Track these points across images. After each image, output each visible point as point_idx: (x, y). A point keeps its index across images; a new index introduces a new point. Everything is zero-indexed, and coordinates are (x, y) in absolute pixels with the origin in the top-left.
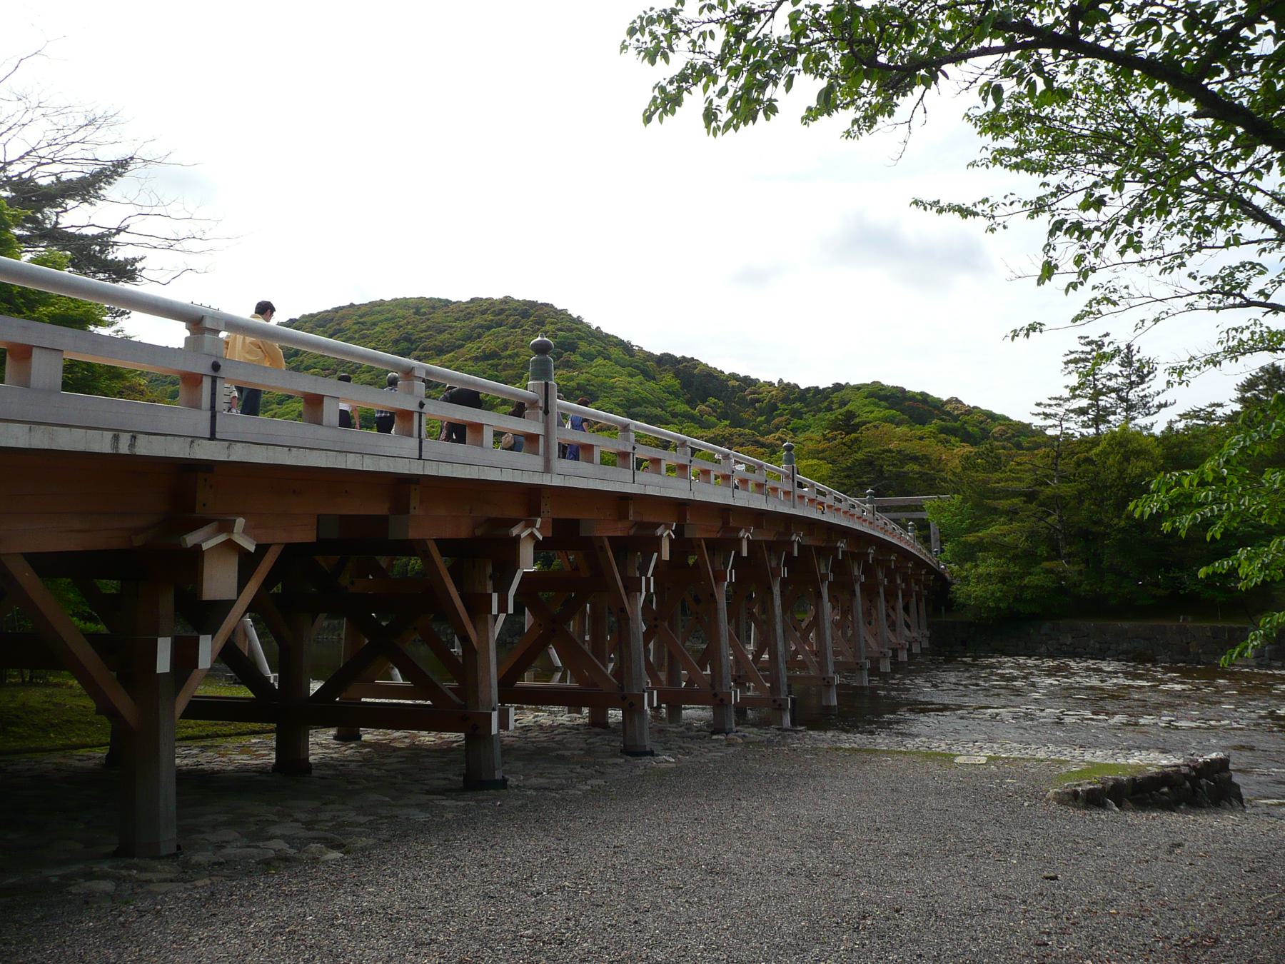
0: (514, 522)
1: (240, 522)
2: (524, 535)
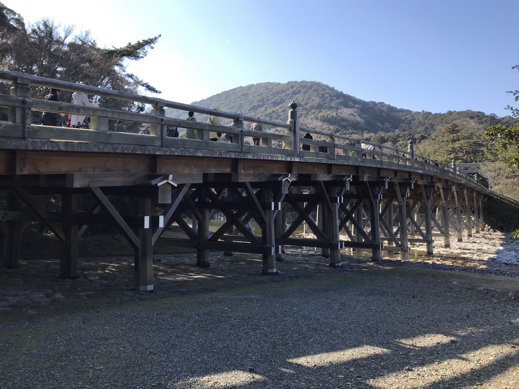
0: (279, 175)
1: (171, 177)
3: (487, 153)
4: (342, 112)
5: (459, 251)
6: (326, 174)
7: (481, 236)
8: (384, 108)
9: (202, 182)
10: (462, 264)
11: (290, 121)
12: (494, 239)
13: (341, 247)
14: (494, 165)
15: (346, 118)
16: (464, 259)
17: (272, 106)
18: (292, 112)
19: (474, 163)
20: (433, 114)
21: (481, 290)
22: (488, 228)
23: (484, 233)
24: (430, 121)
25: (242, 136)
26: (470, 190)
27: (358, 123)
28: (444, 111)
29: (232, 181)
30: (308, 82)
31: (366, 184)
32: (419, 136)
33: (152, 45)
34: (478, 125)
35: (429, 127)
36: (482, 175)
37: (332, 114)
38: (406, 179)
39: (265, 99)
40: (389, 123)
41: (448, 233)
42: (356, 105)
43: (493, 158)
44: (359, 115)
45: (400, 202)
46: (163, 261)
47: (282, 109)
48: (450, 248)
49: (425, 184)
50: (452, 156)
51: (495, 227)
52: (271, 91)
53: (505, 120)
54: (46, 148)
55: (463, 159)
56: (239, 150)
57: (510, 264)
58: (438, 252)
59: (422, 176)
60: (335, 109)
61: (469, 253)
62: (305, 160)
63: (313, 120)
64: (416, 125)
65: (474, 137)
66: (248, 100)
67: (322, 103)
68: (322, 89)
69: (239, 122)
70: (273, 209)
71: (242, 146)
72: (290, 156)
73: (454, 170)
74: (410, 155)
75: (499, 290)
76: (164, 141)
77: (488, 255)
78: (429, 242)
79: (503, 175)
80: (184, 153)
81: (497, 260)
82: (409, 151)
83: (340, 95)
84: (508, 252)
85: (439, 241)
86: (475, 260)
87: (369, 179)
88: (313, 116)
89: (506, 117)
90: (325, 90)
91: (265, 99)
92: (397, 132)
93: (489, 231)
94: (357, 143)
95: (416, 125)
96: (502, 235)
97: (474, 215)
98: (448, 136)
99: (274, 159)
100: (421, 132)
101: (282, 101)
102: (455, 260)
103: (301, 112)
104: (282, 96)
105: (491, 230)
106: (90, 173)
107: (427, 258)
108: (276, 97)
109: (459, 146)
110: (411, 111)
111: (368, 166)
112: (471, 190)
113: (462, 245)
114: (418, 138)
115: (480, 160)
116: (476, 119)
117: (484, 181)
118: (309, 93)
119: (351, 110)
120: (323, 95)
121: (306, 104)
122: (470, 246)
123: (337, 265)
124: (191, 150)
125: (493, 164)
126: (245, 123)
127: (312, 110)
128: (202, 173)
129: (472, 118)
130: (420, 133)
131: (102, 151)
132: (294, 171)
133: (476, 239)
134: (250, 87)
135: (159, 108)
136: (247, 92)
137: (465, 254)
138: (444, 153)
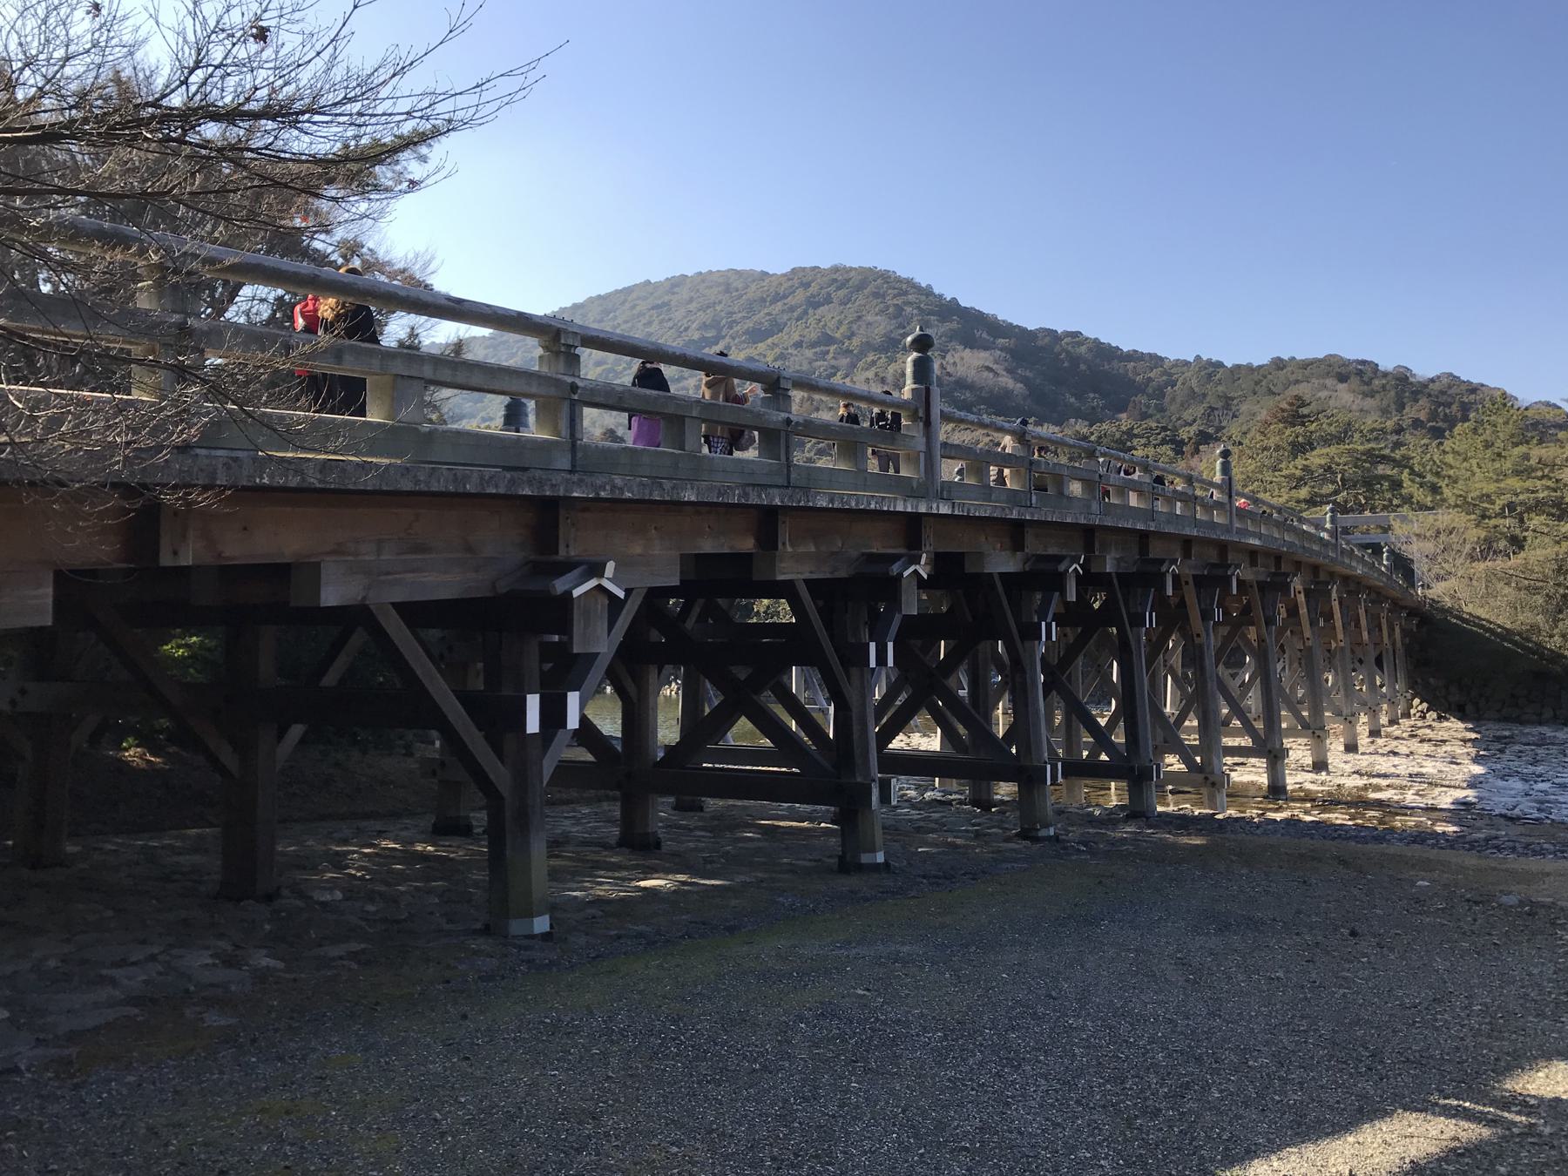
0: (894, 558)
1: (610, 568)
2: (1070, 570)
3: (1409, 483)
4: (957, 361)
6: (1008, 552)
8: (1083, 349)
9: (678, 584)
10: (1381, 822)
12: (1446, 741)
14: (1431, 519)
15: (969, 380)
16: (1379, 804)
17: (744, 342)
18: (916, 363)
19: (1367, 513)
20: (1229, 365)
21: (1511, 903)
22: (1420, 708)
23: (1412, 723)
24: (1220, 388)
25: (787, 436)
26: (1373, 596)
27: (1007, 393)
28: (1260, 358)
29: (754, 579)
30: (851, 269)
33: (423, 150)
35: (1220, 405)
36: (1400, 549)
38: (1214, 566)
40: (1097, 395)
42: (1001, 341)
43: (1429, 499)
44: (1008, 371)
47: (777, 351)
48: (1328, 773)
49: (1262, 578)
50: (1304, 493)
51: (1446, 706)
52: (740, 296)
53: (1435, 387)
54: (266, 481)
55: (1334, 502)
56: (781, 481)
57: (1519, 818)
58: (1298, 786)
59: (1253, 555)
61: (1388, 786)
62: (966, 510)
63: (871, 381)
64: (1179, 400)
65: (1357, 436)
66: (670, 324)
67: (895, 335)
68: (896, 291)
69: (780, 391)
71: (789, 467)
72: (915, 497)
74: (1222, 492)
76: (579, 455)
77: (1446, 792)
80: (647, 491)
81: (1478, 807)
82: (1218, 478)
83: (950, 310)
84: (1501, 783)
85: (1299, 752)
86: (1413, 808)
88: (870, 374)
89: (1439, 377)
90: (906, 293)
92: (1125, 421)
93: (1424, 718)
94: (1087, 458)
95: (1179, 400)
97: (1383, 672)
98: (1281, 432)
99: (885, 509)
101: (776, 327)
102: (1355, 808)
103: (833, 362)
104: (774, 312)
106: (367, 558)
107: (1271, 806)
109: (1323, 462)
110: (1161, 359)
111: (1125, 526)
112: (1377, 595)
113: (1363, 762)
114: (1190, 439)
116: (1355, 381)
117: (1403, 565)
118: (857, 304)
119: (984, 354)
120: (899, 309)
122: (1384, 765)
123: (1043, 833)
124: (667, 484)
125: (1428, 518)
126: (797, 395)
127: (866, 356)
128: (678, 553)
129: (1343, 378)
130: (1191, 425)
131: (426, 489)
132: (928, 546)
133: (1395, 743)
134: (676, 283)
135: (563, 349)
136: (666, 298)
137: (1378, 789)
138: (1279, 484)
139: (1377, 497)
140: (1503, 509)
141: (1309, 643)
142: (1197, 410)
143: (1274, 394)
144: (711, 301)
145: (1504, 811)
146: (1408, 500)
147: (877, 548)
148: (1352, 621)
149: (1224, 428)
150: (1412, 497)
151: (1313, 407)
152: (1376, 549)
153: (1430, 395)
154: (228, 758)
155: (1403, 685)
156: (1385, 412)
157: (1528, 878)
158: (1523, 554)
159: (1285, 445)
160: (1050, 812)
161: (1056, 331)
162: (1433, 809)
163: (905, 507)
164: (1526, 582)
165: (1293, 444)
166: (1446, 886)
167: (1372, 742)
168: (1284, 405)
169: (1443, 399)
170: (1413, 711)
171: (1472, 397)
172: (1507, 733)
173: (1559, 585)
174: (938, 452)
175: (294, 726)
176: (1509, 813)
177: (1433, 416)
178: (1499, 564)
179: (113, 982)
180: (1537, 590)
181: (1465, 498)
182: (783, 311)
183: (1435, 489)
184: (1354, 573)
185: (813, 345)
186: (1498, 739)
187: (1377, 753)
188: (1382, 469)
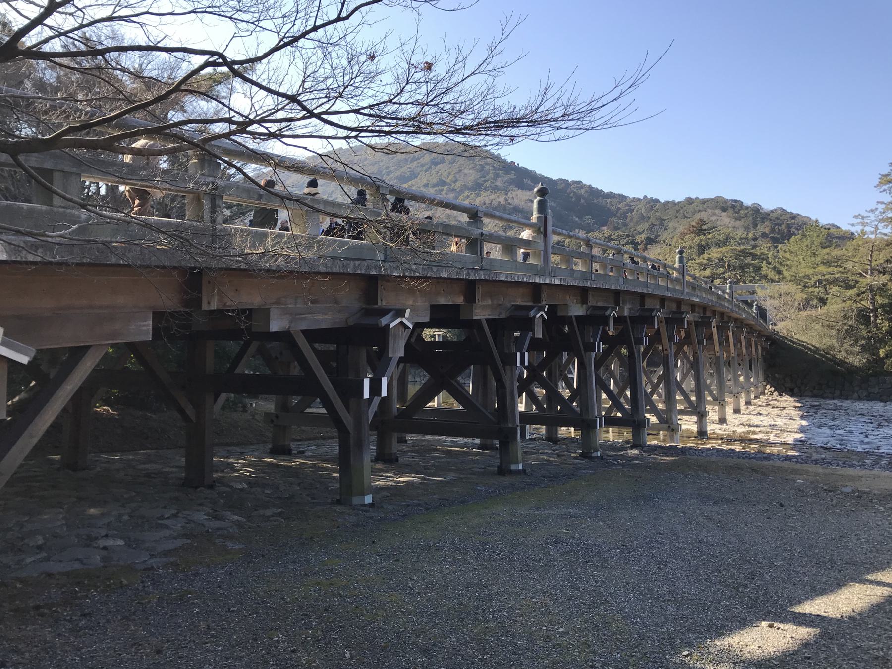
0: (530, 308)
2: (537, 316)
5: (745, 429)
7: (764, 404)
8: (583, 191)
11: (537, 217)
13: (601, 426)
16: (756, 441)
18: (540, 203)
19: (741, 284)
21: (848, 491)
22: (770, 390)
23: (766, 398)
24: (658, 214)
25: (481, 242)
28: (679, 197)
31: (626, 321)
32: (643, 239)
34: (735, 221)
35: (657, 223)
36: (760, 304)
37: (498, 200)
38: (674, 312)
39: (384, 172)
41: (724, 400)
43: (777, 277)
45: (666, 350)
46: (308, 454)
48: (727, 425)
49: (696, 319)
51: (782, 389)
53: (775, 215)
57: (830, 449)
58: (712, 431)
59: (693, 306)
60: (503, 192)
61: (760, 431)
64: (635, 220)
65: (733, 241)
67: (480, 181)
70: (366, 395)
73: (730, 297)
74: (679, 273)
75: (876, 492)
78: (702, 415)
79: (792, 306)
82: (677, 265)
84: (818, 430)
85: (713, 414)
87: (630, 313)
89: (775, 210)
91: (384, 172)
93: (772, 395)
96: (795, 401)
99: (531, 281)
100: (643, 232)
105: (776, 394)
106: (290, 306)
108: (404, 169)
109: (718, 256)
110: (625, 197)
112: (751, 329)
113: (745, 419)
114: (642, 242)
115: (751, 280)
116: (731, 211)
117: (762, 313)
118: (459, 163)
120: (482, 167)
121: (455, 182)
122: (756, 420)
123: (594, 455)
124: (435, 269)
126: (486, 220)
127: (464, 193)
128: (428, 304)
129: (724, 209)
130: (641, 234)
133: (759, 409)
137: (754, 433)
139: (746, 275)
140: (815, 283)
141: (717, 355)
142: (645, 226)
143: (687, 217)
144: (377, 160)
145: (822, 445)
146: (765, 277)
147: (519, 302)
148: (738, 342)
149: (660, 236)
150: (767, 276)
151: (709, 225)
152: (750, 305)
153: (770, 220)
154: (190, 411)
155: (394, 407)
156: (747, 228)
157: (852, 479)
158: (826, 307)
159: (695, 245)
160: (598, 445)
161: (568, 181)
162: (785, 443)
163: (540, 280)
164: (827, 323)
165: (699, 246)
166: (812, 482)
167: (747, 408)
168: (694, 224)
169: (777, 222)
170: (766, 392)
171: (793, 221)
172: (817, 404)
173: (845, 324)
174: (550, 250)
175: (222, 394)
176: (825, 446)
177: (772, 231)
178: (813, 313)
179: (167, 527)
180: (833, 327)
181: (796, 276)
182: (418, 166)
183: (780, 272)
184: (741, 317)
185: (435, 186)
186: (813, 407)
187: (751, 414)
188: (749, 260)
